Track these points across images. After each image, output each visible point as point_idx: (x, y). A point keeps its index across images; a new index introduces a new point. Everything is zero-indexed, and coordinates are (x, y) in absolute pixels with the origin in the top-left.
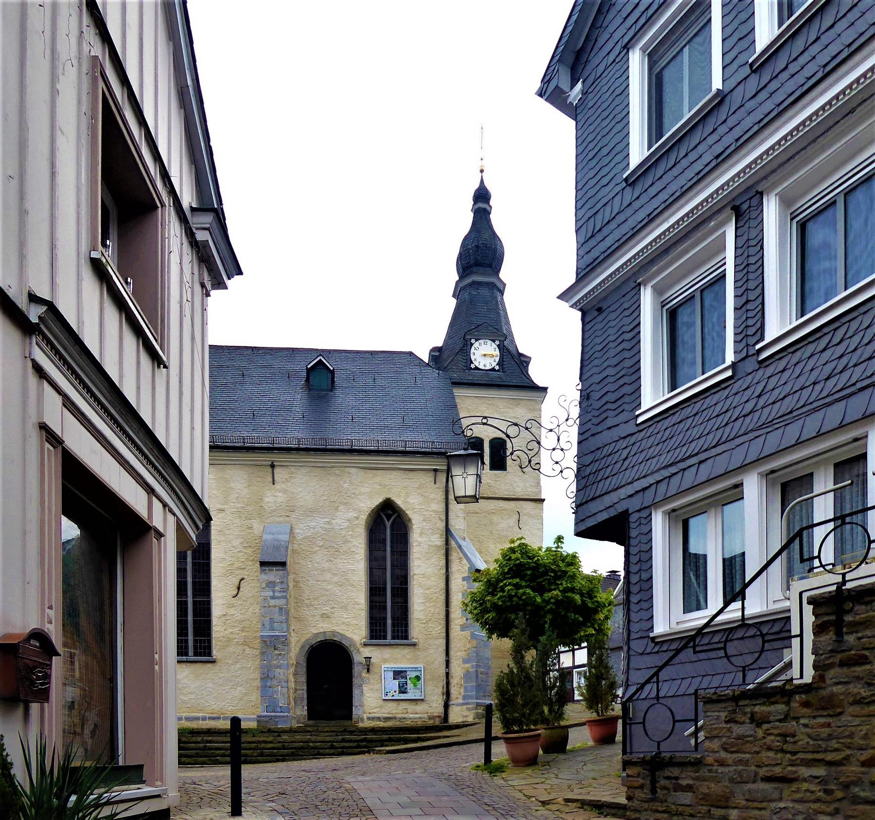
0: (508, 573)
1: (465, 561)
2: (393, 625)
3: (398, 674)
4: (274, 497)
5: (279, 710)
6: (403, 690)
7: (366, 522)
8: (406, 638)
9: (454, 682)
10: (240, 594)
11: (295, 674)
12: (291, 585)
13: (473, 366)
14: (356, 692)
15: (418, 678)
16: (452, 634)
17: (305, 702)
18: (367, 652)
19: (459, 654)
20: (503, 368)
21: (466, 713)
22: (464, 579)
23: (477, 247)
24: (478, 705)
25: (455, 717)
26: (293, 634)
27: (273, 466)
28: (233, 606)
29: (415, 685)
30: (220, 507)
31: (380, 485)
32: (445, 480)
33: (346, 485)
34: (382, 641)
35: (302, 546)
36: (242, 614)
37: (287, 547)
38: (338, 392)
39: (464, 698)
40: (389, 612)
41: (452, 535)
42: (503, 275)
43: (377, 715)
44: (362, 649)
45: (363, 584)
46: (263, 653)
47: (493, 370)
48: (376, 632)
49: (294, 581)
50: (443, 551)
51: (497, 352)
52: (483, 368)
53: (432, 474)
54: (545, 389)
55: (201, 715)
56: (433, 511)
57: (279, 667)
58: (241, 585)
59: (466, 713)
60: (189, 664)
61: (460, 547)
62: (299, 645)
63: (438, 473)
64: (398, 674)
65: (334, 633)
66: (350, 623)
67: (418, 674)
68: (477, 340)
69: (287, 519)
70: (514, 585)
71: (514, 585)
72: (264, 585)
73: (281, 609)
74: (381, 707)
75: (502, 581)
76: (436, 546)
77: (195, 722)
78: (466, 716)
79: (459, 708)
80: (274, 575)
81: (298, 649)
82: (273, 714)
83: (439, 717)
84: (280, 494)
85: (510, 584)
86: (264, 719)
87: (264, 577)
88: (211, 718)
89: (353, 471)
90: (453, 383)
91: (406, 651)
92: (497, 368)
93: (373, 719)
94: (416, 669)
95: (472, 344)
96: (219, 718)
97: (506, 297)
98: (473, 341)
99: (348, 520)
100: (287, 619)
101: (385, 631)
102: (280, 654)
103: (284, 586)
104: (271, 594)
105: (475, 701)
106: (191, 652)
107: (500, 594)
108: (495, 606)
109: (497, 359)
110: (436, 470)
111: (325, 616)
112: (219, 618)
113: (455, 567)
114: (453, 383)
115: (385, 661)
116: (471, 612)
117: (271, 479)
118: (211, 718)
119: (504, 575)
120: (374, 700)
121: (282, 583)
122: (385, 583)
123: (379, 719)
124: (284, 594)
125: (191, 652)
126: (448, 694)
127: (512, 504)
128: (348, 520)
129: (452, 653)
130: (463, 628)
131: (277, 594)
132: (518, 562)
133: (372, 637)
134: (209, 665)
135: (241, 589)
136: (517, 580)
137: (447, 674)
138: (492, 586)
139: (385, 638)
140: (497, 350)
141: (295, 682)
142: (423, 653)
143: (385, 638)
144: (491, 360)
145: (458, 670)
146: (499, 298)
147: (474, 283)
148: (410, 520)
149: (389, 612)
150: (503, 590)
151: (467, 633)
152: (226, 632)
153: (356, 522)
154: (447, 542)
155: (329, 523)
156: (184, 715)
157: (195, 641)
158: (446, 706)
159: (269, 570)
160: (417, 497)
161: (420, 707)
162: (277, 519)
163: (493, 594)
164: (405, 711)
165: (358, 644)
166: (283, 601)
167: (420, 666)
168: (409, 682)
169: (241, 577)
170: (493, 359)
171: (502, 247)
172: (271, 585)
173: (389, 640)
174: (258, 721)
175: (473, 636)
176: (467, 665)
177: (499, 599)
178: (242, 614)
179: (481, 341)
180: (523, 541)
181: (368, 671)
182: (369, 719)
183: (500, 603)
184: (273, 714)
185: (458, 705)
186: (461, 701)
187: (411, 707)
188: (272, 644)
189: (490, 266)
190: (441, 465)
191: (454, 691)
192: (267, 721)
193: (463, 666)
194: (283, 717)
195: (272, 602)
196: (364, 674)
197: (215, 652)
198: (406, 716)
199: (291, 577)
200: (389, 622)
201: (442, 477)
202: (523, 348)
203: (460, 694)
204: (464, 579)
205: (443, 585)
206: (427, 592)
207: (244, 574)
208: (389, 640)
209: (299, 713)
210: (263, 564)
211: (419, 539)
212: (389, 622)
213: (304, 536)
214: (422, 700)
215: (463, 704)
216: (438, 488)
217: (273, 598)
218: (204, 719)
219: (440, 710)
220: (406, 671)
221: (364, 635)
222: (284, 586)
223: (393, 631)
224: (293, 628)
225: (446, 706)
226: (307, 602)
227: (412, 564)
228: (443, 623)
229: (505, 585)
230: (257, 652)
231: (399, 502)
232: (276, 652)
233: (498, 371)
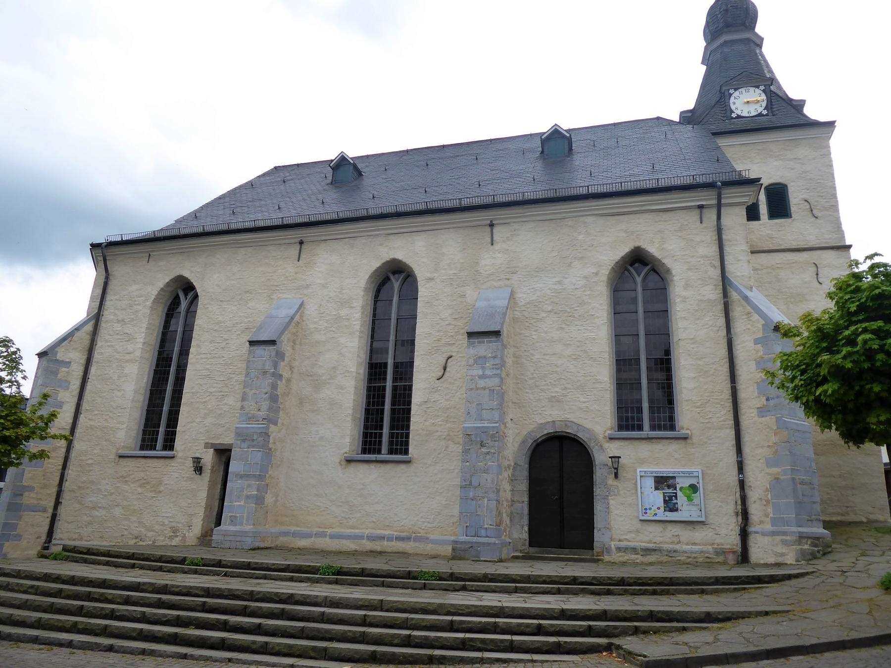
0: (856, 313)
1: (756, 317)
2: (651, 408)
3: (662, 482)
4: (491, 259)
5: (483, 533)
6: (670, 505)
7: (609, 278)
8: (672, 428)
9: (753, 496)
10: (447, 374)
11: (512, 480)
12: (509, 361)
13: (734, 115)
14: (598, 507)
15: (694, 488)
16: (745, 422)
17: (526, 520)
18: (614, 448)
19: (759, 451)
20: (772, 112)
21: (780, 549)
22: (756, 341)
23: (727, 10)
24: (802, 537)
25: (765, 550)
26: (510, 424)
27: (492, 225)
28: (437, 391)
29: (690, 499)
30: (428, 275)
31: (626, 232)
32: (715, 217)
33: (581, 237)
34: (372, 457)
35: (526, 314)
36: (447, 400)
37: (505, 314)
38: (575, 157)
39: (774, 522)
40: (646, 392)
41: (731, 284)
42: (759, 29)
43: (632, 544)
44: (606, 445)
45: (606, 355)
46: (466, 452)
47: (760, 115)
48: (628, 420)
49: (514, 355)
50: (721, 307)
51: (764, 97)
52: (747, 115)
53: (697, 211)
54: (831, 125)
55: (386, 533)
56: (702, 257)
57: (486, 471)
58: (449, 365)
59: (780, 549)
60: (378, 465)
61: (746, 298)
62: (519, 440)
63: (704, 210)
64: (662, 482)
65: (567, 422)
66: (591, 411)
67: (693, 481)
68: (736, 90)
69: (507, 282)
70: (873, 332)
71: (873, 332)
72: (471, 362)
73: (492, 391)
74: (637, 531)
75: (847, 328)
76: (709, 300)
77: (378, 543)
78: (782, 555)
79: (767, 540)
80: (485, 348)
81: (517, 445)
82: (475, 539)
83: (734, 552)
84: (499, 255)
85: (865, 330)
86: (463, 547)
87: (472, 351)
88: (399, 539)
89: (590, 219)
90: (714, 134)
91: (673, 448)
92: (765, 112)
93: (625, 550)
94: (689, 475)
95: (731, 95)
96: (408, 539)
97: (765, 49)
98: (731, 91)
99: (585, 277)
100: (501, 405)
101: (641, 419)
102: (488, 453)
103: (498, 361)
104: (480, 372)
105: (794, 529)
106: (385, 447)
107: (845, 350)
108: (838, 373)
109: (764, 104)
110: (701, 207)
111: (555, 400)
112: (420, 405)
113: (739, 326)
114: (714, 134)
115: (641, 462)
116: (782, 386)
117: (489, 240)
118: (399, 539)
119: (849, 317)
120: (626, 517)
121: (494, 357)
122: (638, 352)
123: (634, 550)
124: (498, 372)
125: (385, 447)
126: (745, 514)
127: (805, 256)
128: (585, 277)
129: (747, 449)
130: (762, 411)
131: (488, 372)
132: (877, 291)
133: (620, 428)
134: (403, 466)
135: (448, 369)
136: (880, 323)
137: (742, 484)
138: (826, 337)
139: (640, 428)
140: (763, 94)
141: (512, 490)
142: (701, 448)
143: (640, 428)
144: (757, 106)
145: (758, 477)
146: (758, 51)
147: (726, 42)
148: (668, 271)
149: (646, 392)
150: (851, 342)
151: (770, 420)
152: (427, 423)
153: (596, 279)
154: (725, 294)
155: (559, 283)
156: (367, 532)
157: (391, 435)
158: (744, 534)
159: (479, 342)
160: (679, 242)
161: (699, 535)
162: (495, 284)
163: (829, 350)
164: (676, 540)
165: (601, 437)
166: (497, 381)
167: (697, 469)
168: (679, 494)
169: (448, 354)
170: (759, 104)
171: (754, 6)
172: (480, 360)
173: (646, 432)
174: (454, 549)
175: (781, 425)
176: (775, 470)
177: (844, 358)
178: (447, 400)
179: (743, 90)
180: (877, 260)
181: (616, 476)
182: (619, 549)
183: (849, 365)
184: (475, 539)
185: (764, 534)
186: (768, 527)
187: (685, 534)
188: (479, 441)
189: (743, 24)
190: (708, 198)
191: (755, 510)
192: (465, 550)
193: (768, 470)
194: (489, 544)
195: (482, 383)
196: (611, 481)
197: (411, 449)
198: (677, 547)
199: (509, 351)
200: (645, 405)
201: (711, 215)
202: (793, 93)
203: (767, 516)
204: (756, 341)
205: (723, 351)
206: (699, 362)
207: (453, 350)
208: (646, 432)
209: (516, 535)
210: (471, 335)
211: (684, 294)
212: (645, 405)
213: (528, 300)
214: (702, 523)
215: (773, 534)
216: (706, 227)
217: (482, 377)
218: (390, 539)
219: (732, 540)
220: (674, 477)
221: (609, 425)
222: (498, 361)
223: (652, 419)
224: (511, 416)
225: (744, 534)
226: (531, 382)
227: (674, 327)
228: (729, 405)
229: (856, 334)
230: (460, 449)
231: (653, 249)
232: (484, 450)
233: (767, 115)
